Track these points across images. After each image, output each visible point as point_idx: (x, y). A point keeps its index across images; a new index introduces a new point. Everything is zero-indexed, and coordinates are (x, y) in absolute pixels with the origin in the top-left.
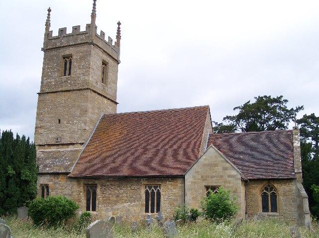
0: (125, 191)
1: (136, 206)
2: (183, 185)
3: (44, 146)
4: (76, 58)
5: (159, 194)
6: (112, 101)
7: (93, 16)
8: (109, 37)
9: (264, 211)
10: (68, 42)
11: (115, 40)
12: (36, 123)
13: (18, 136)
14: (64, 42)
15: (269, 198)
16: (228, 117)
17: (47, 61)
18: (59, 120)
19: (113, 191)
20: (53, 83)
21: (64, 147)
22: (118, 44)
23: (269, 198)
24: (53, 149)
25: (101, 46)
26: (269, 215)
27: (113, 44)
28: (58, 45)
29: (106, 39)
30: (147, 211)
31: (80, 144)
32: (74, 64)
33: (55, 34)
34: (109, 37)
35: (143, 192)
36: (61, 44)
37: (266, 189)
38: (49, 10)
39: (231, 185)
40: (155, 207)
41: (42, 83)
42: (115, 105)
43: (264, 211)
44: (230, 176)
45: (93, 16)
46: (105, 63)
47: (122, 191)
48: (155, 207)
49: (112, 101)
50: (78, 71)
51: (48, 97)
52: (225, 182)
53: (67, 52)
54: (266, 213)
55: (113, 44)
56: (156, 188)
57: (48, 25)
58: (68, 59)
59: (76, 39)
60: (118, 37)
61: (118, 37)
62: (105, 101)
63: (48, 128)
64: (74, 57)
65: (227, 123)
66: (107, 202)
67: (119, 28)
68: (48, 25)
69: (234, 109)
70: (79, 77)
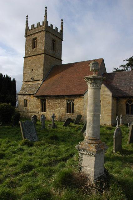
4: (46, 41)
5: (73, 103)
6: (59, 59)
7: (46, 16)
8: (56, 27)
9: (127, 114)
11: (59, 29)
13: (4, 75)
14: (34, 31)
15: (130, 107)
16: (122, 66)
17: (27, 41)
18: (32, 70)
22: (61, 31)
23: (130, 107)
24: (31, 83)
25: (51, 32)
26: (129, 116)
27: (59, 31)
28: (31, 33)
29: (54, 28)
31: (41, 80)
32: (38, 42)
33: (30, 28)
34: (56, 27)
35: (65, 103)
37: (129, 102)
38: (27, 16)
39: (107, 100)
40: (71, 108)
41: (25, 52)
43: (127, 114)
44: (106, 95)
45: (46, 16)
46: (53, 41)
48: (71, 108)
49: (59, 59)
52: (104, 98)
53: (35, 36)
54: (128, 115)
55: (59, 31)
56: (71, 101)
57: (27, 24)
58: (35, 39)
59: (39, 29)
60: (62, 27)
61: (62, 27)
62: (55, 59)
64: (38, 38)
65: (122, 68)
67: (62, 22)
68: (27, 24)
69: (124, 61)
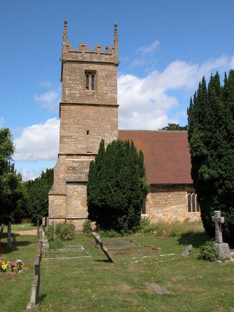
0: (172, 196)
1: (182, 207)
2: (36, 277)
3: (72, 155)
10: (91, 58)
12: (60, 133)
19: (162, 196)
20: (78, 95)
21: (70, 157)
30: (189, 211)
36: (83, 58)
42: (115, 109)
47: (170, 196)
50: (105, 88)
51: (66, 107)
53: (91, 67)
59: (101, 58)
63: (76, 138)
66: (156, 205)
70: (106, 94)
